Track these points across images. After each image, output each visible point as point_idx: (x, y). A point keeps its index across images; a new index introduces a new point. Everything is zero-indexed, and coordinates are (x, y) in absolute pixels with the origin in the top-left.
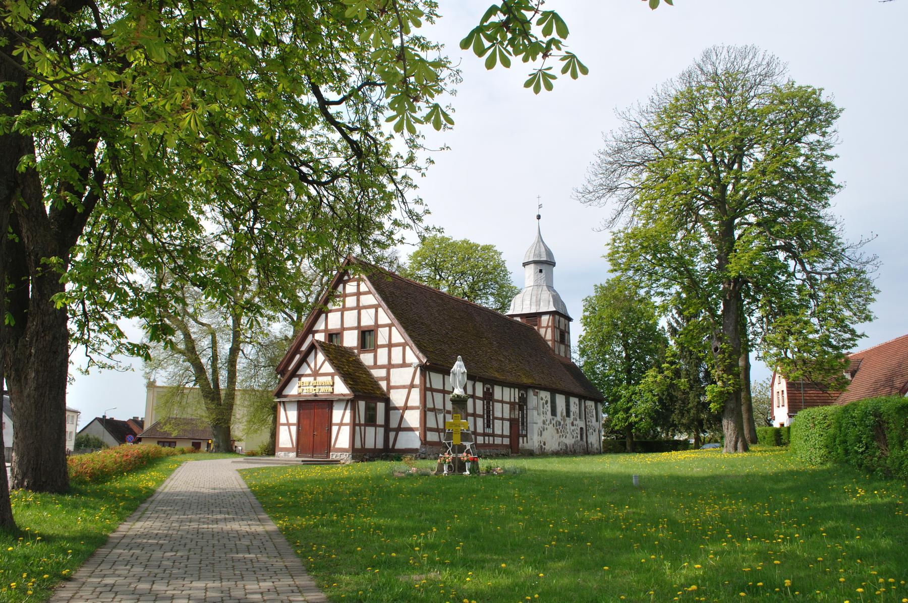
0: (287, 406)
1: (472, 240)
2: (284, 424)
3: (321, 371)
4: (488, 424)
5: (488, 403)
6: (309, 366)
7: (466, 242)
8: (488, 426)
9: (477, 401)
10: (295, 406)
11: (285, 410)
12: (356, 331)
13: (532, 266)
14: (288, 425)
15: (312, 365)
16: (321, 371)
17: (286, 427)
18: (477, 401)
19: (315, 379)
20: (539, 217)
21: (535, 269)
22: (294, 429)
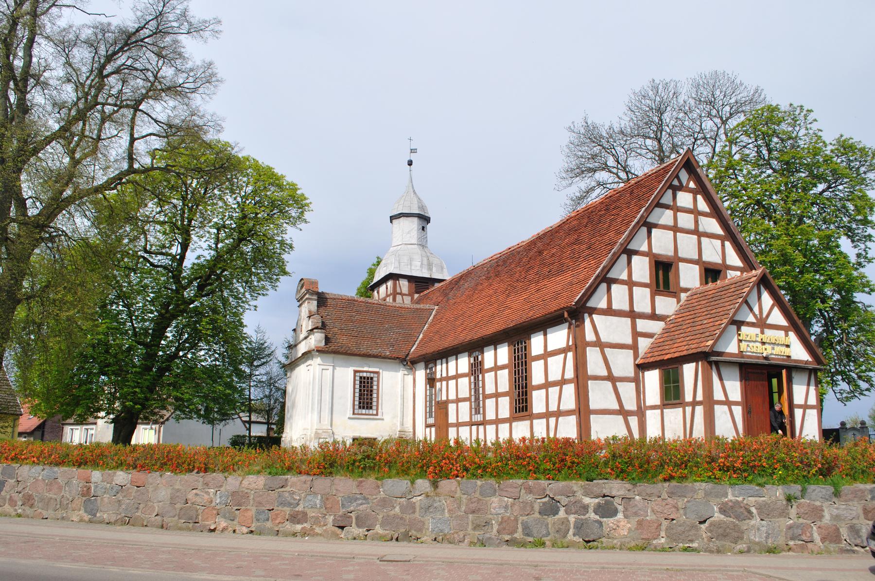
0: (724, 371)
1: (278, 170)
2: (736, 403)
3: (769, 321)
4: (478, 407)
5: (476, 379)
6: (751, 310)
7: (270, 168)
8: (477, 412)
9: (733, 407)
10: (736, 372)
11: (721, 379)
12: (647, 259)
13: (416, 220)
14: (728, 403)
15: (756, 309)
16: (769, 321)
17: (726, 408)
18: (733, 407)
19: (762, 333)
20: (410, 163)
21: (418, 225)
22: (738, 411)
